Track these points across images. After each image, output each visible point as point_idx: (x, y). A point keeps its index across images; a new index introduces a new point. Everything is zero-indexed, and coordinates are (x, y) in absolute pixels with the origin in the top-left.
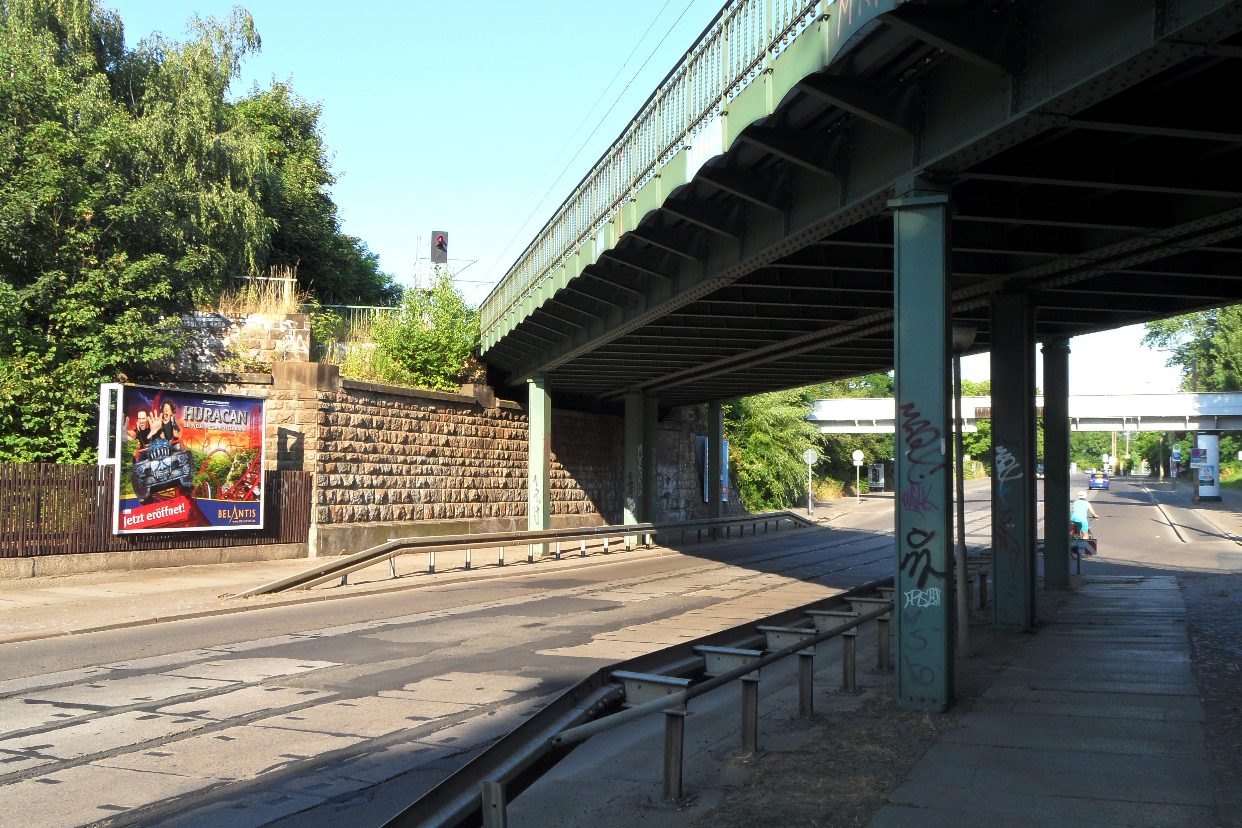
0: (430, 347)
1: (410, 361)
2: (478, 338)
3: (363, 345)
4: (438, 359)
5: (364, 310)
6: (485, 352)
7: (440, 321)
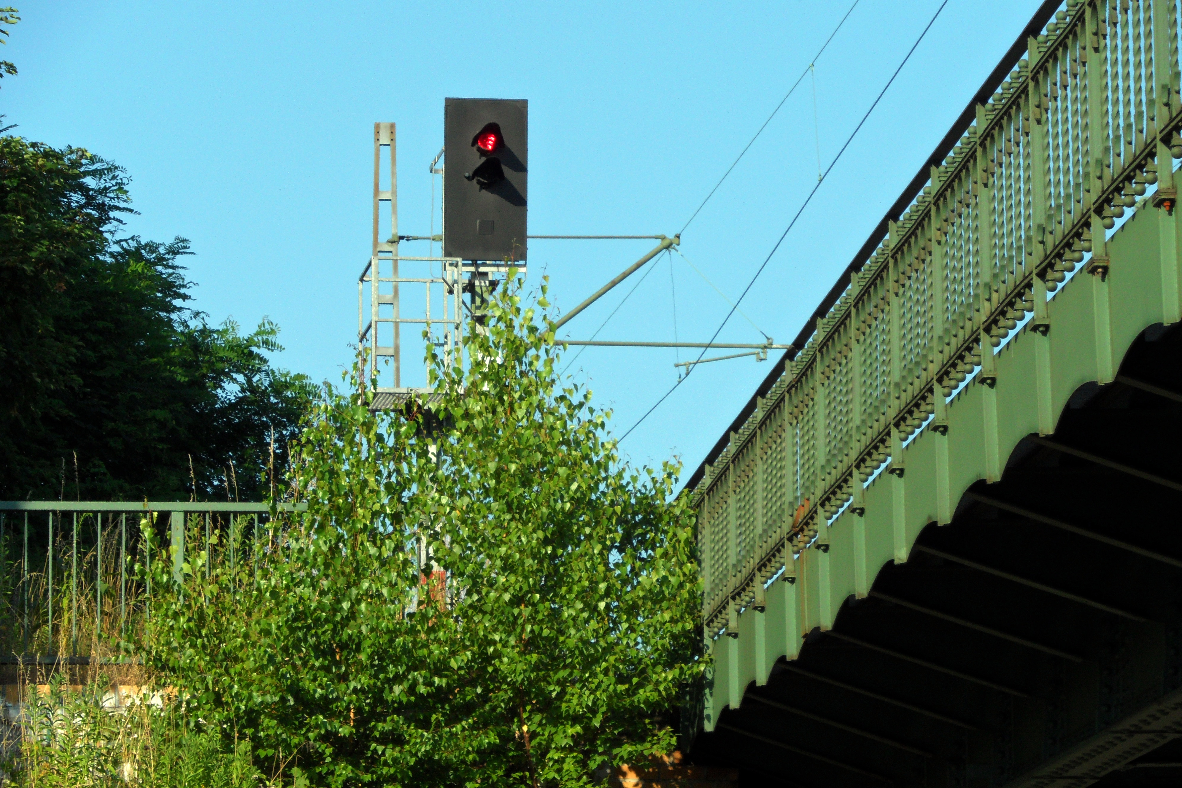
3: (109, 701)
5: (110, 519)
6: (726, 713)
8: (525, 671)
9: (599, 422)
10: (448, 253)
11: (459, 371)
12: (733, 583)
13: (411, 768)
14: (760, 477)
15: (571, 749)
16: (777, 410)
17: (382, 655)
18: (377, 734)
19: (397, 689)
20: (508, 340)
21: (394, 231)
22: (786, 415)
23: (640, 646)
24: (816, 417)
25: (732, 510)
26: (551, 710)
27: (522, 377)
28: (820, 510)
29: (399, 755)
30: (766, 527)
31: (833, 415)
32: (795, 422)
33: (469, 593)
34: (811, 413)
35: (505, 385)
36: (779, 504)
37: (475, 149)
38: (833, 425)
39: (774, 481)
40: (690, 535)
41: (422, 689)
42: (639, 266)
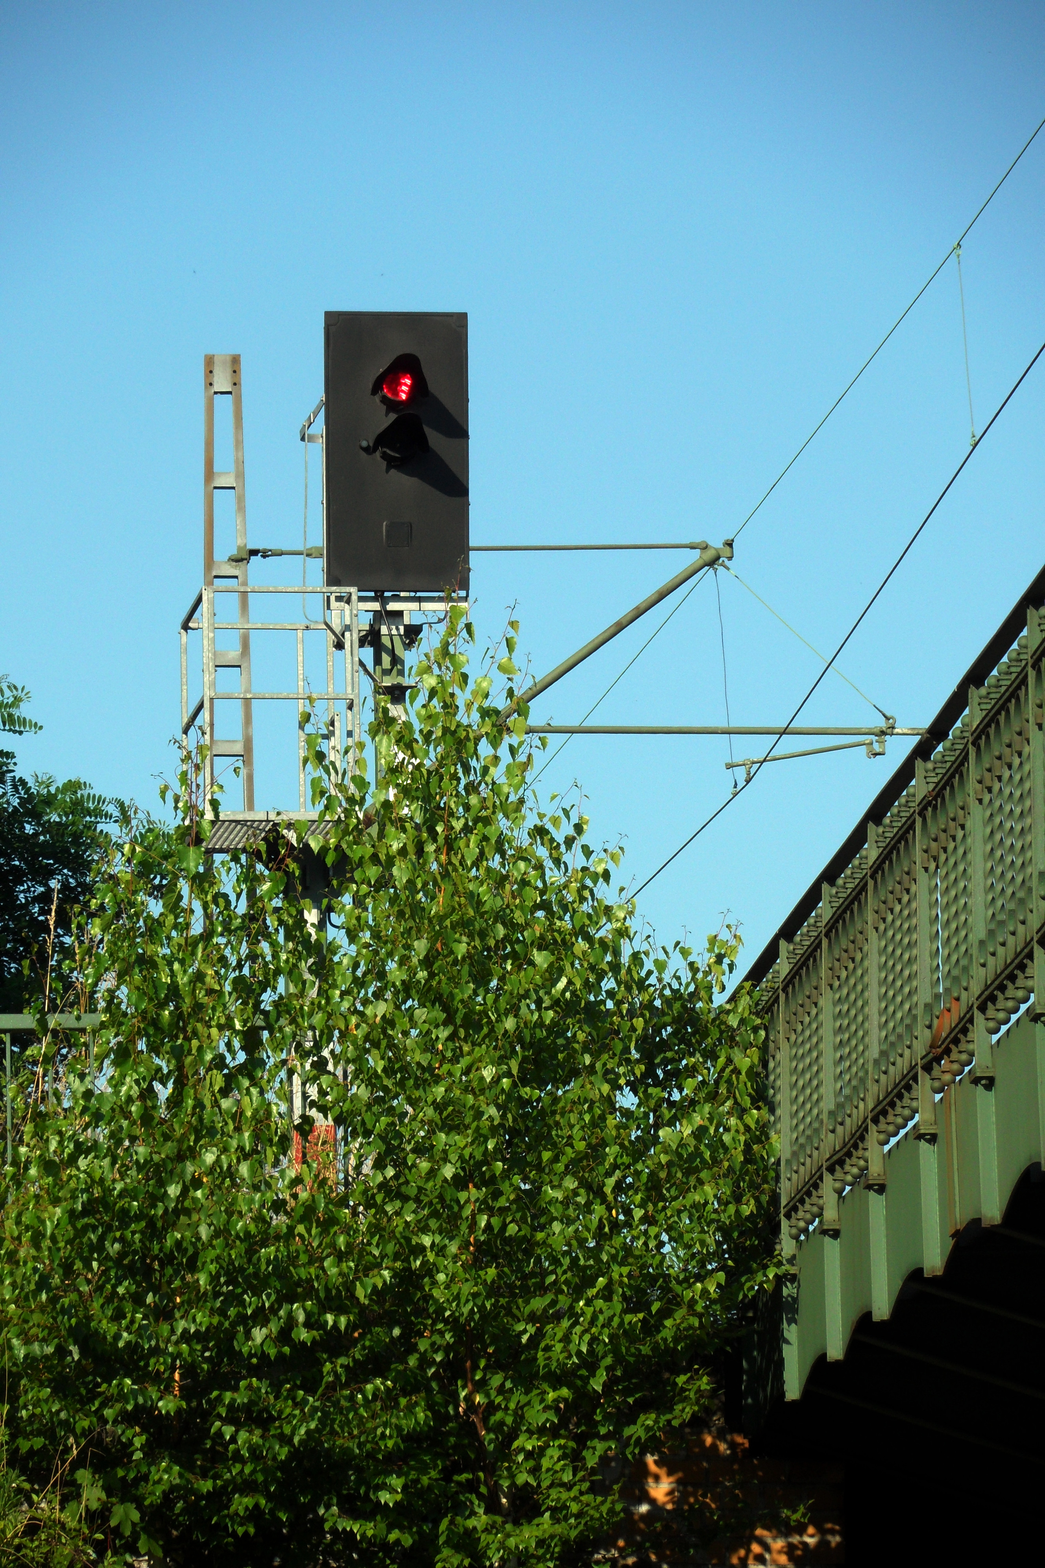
0: (336, 1344)
1: (166, 1474)
2: (752, 1242)
4: (415, 1444)
6: (821, 1370)
7: (416, 1118)
8: (475, 1295)
9: (600, 869)
10: (333, 580)
11: (361, 783)
12: (830, 1142)
13: (283, 1466)
14: (873, 961)
15: (554, 1432)
16: (902, 846)
17: (238, 1277)
18: (223, 1412)
19: (259, 1334)
20: (446, 730)
21: (240, 542)
22: (918, 855)
23: (667, 1249)
24: (969, 856)
25: (826, 1017)
26: (518, 1363)
27: (468, 793)
28: (979, 1017)
29: (261, 1442)
30: (884, 1047)
31: (998, 854)
32: (933, 866)
33: (379, 1165)
34: (961, 851)
35: (438, 807)
36: (907, 1006)
37: (377, 399)
38: (999, 870)
39: (898, 968)
40: (756, 1061)
41: (303, 1335)
42: (661, 596)
